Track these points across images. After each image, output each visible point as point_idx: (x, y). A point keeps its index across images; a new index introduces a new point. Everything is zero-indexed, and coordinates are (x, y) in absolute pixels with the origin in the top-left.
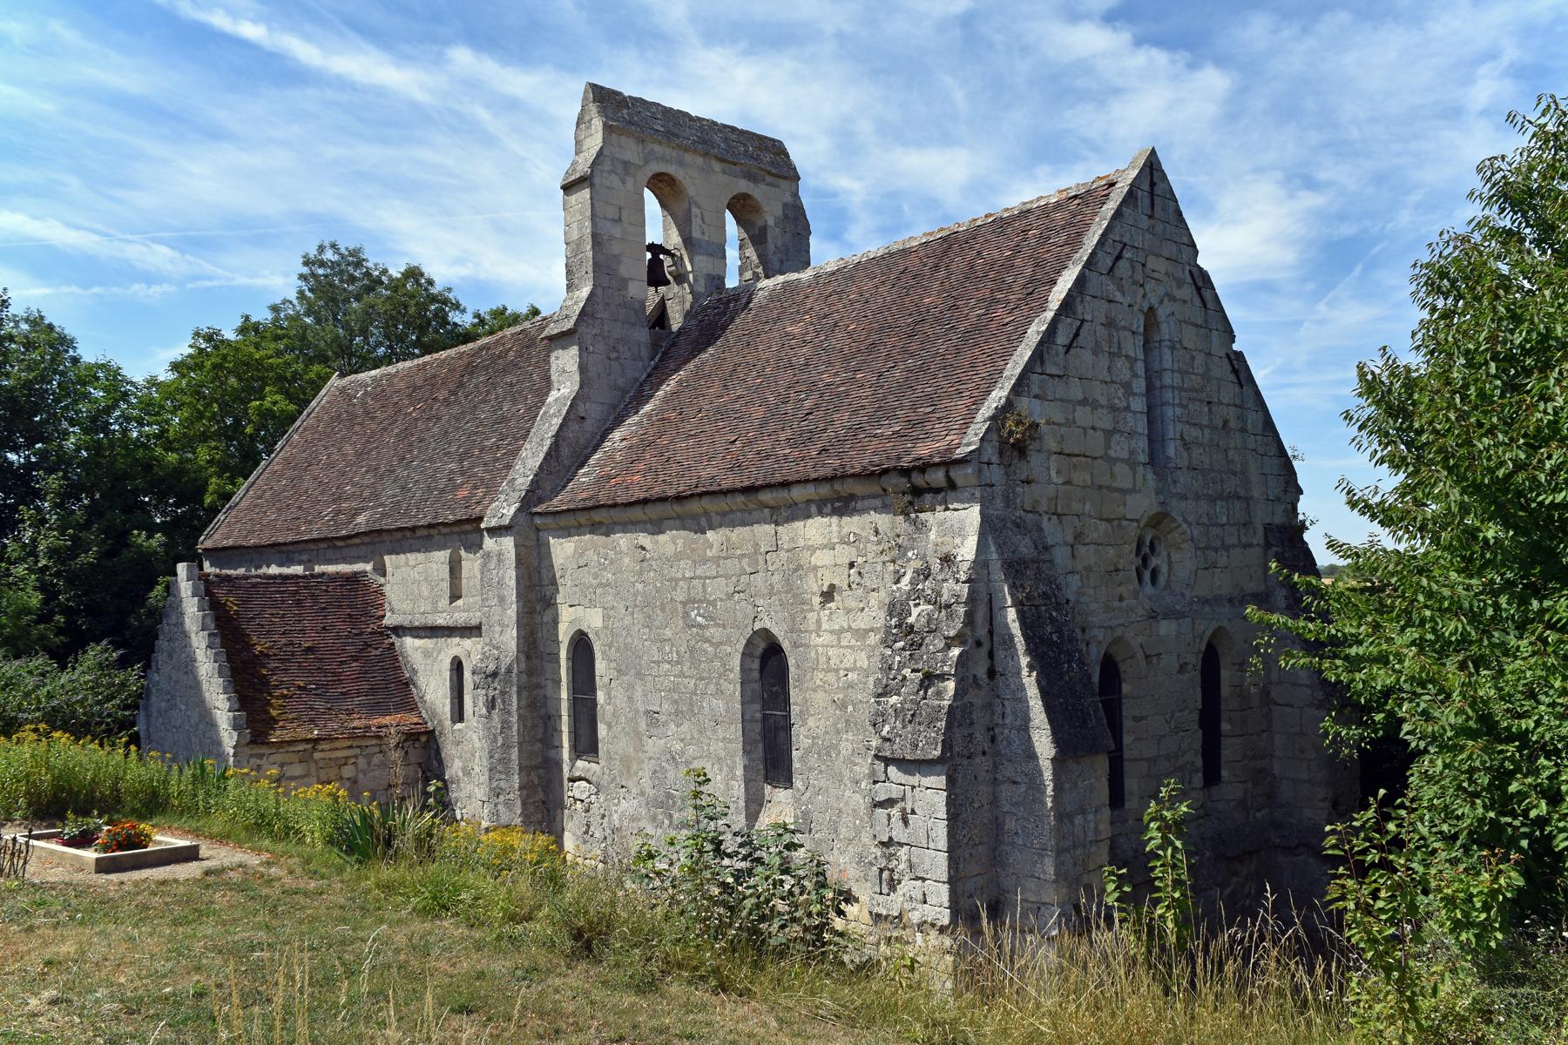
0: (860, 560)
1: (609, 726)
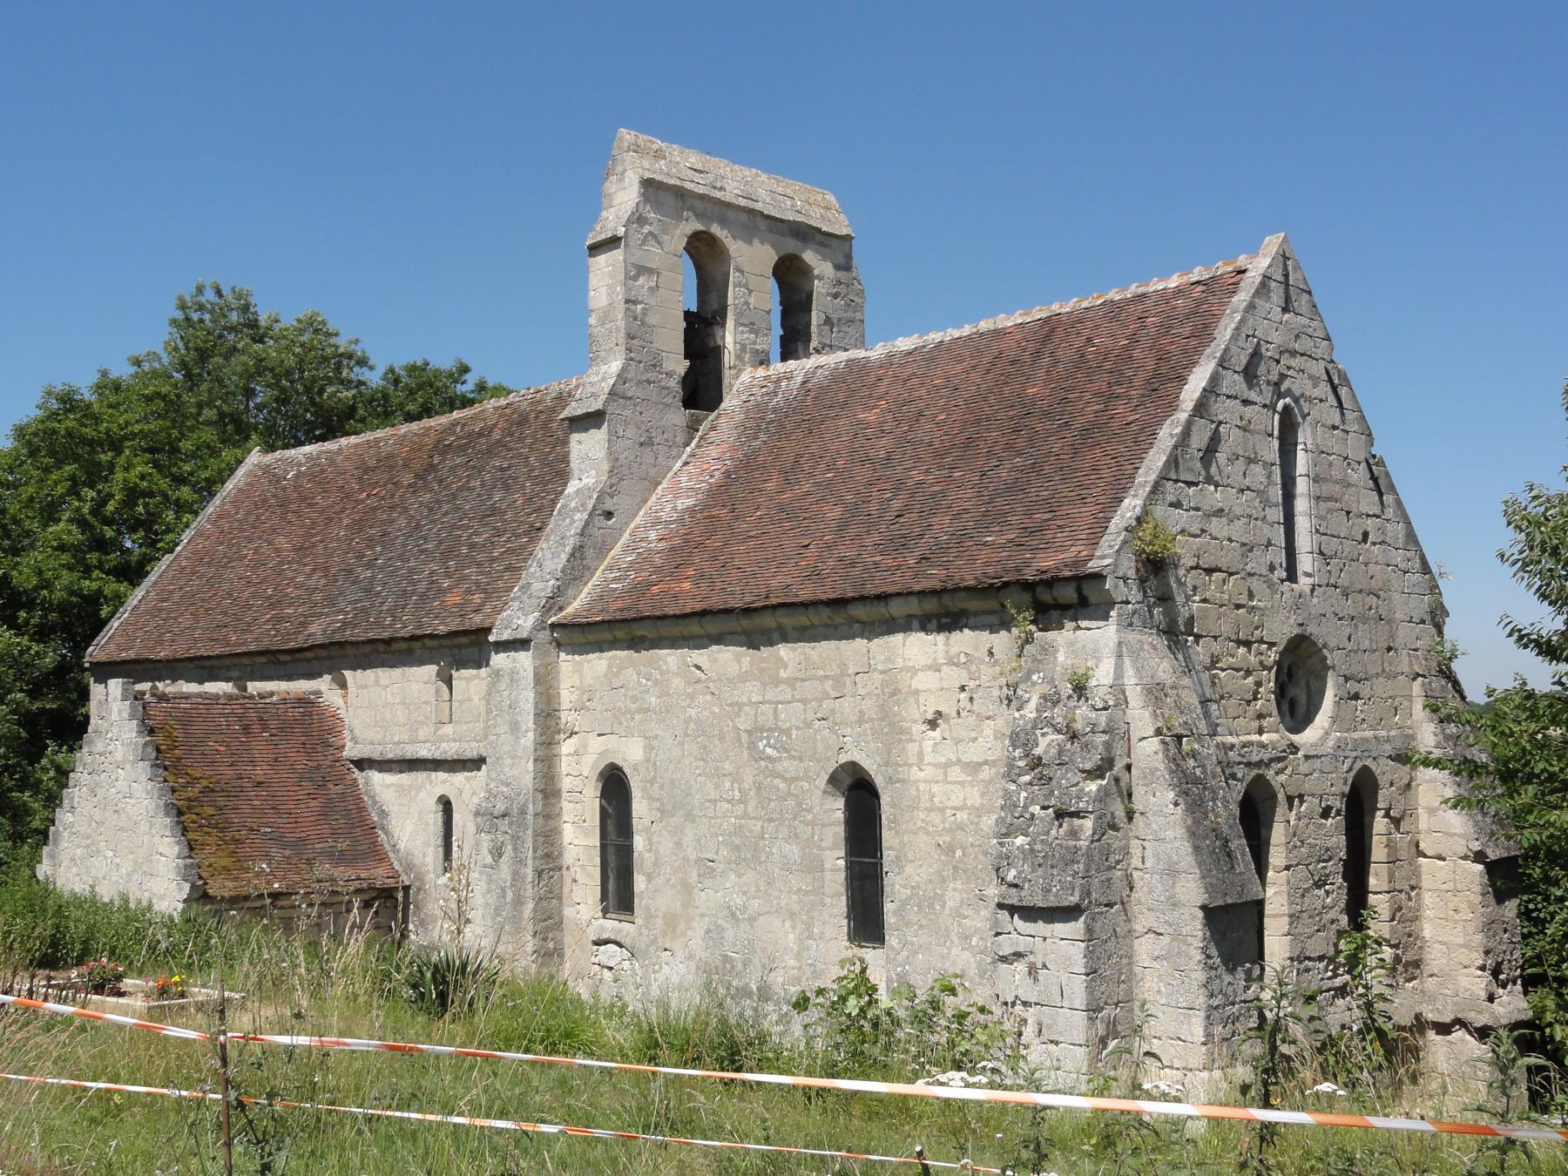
0: (972, 684)
1: (650, 878)
